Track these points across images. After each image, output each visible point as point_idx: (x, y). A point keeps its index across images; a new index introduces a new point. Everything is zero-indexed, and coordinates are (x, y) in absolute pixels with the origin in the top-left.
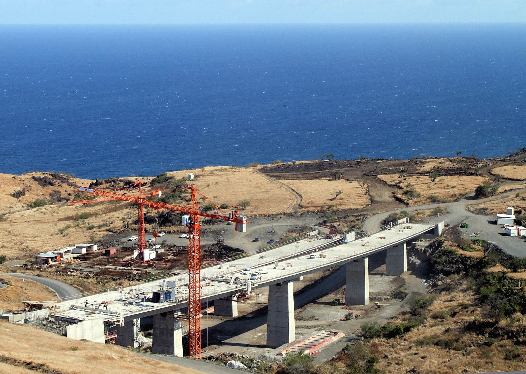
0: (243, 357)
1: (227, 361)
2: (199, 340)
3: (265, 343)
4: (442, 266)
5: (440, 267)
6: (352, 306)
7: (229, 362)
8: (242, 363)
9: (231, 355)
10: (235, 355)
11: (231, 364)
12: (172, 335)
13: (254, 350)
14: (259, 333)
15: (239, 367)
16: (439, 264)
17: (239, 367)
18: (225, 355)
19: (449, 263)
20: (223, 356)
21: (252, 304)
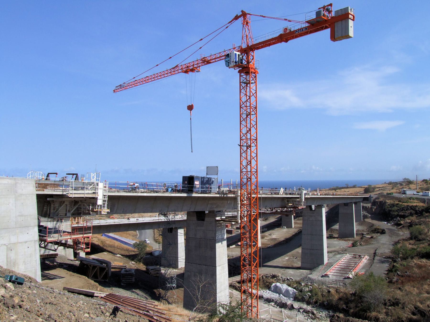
0: (288, 279)
1: (271, 283)
2: (256, 256)
3: (299, 264)
4: (397, 213)
5: (396, 213)
6: (347, 239)
7: (274, 284)
8: (289, 285)
9: (274, 276)
10: (278, 276)
11: (276, 287)
12: (213, 249)
13: (291, 271)
14: (294, 256)
15: (287, 291)
16: (394, 211)
17: (287, 291)
18: (266, 277)
19: (402, 210)
20: (264, 277)
21: (268, 240)
